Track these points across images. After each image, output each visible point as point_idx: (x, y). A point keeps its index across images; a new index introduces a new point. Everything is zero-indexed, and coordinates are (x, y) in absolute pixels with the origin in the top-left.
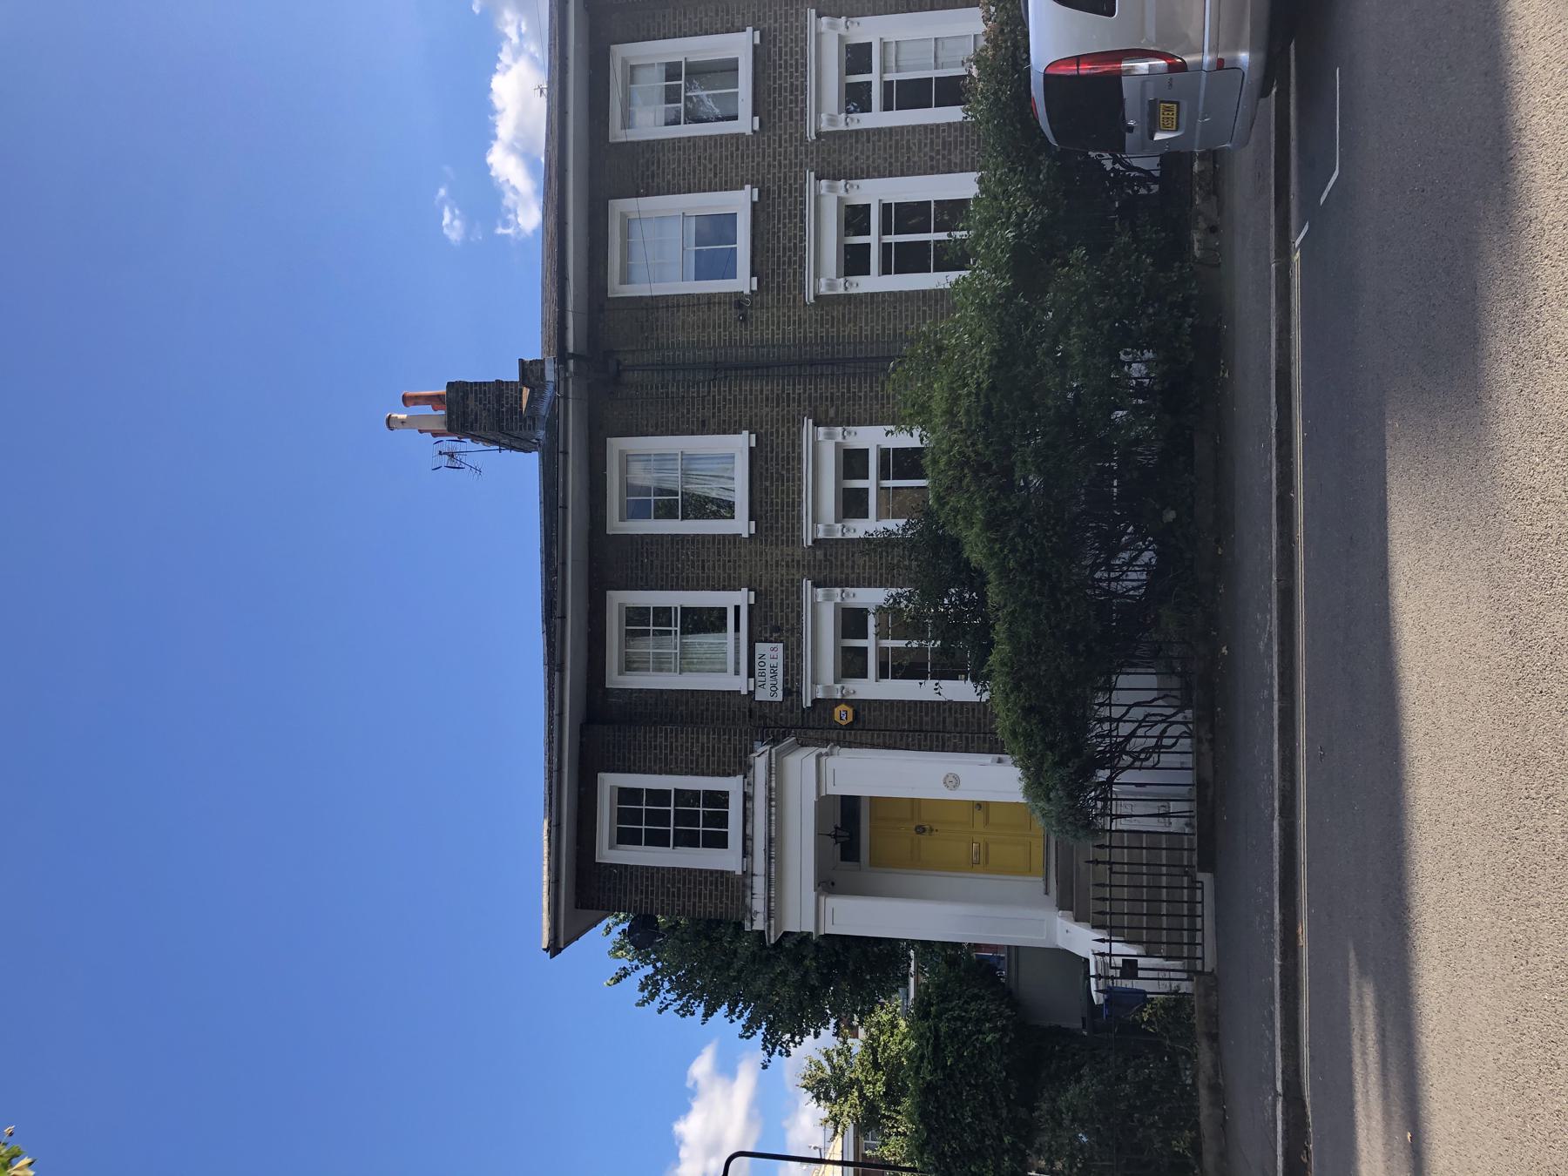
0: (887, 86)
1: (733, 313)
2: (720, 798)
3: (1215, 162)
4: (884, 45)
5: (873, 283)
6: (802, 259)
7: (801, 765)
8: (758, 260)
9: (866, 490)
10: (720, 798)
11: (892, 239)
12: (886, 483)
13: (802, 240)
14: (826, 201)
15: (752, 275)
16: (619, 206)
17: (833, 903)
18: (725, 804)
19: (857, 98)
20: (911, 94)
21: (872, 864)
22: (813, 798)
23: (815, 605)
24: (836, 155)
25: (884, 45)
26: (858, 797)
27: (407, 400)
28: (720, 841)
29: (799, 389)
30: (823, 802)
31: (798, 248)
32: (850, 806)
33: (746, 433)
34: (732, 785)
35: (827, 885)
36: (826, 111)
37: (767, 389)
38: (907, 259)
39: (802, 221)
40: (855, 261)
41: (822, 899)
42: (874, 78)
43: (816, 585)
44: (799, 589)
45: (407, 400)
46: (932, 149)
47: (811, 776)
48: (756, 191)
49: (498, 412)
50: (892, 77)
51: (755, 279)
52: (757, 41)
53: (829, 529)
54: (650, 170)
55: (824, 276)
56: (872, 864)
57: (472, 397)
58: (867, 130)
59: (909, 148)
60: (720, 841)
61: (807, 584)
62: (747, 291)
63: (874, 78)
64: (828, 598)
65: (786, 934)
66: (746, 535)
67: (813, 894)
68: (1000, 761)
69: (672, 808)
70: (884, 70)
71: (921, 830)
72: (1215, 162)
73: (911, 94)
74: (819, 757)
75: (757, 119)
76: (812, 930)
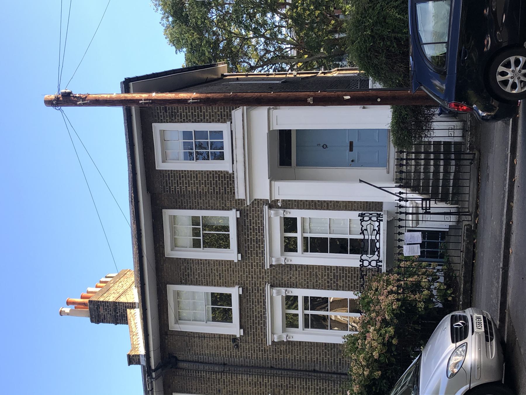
0: (305, 239)
1: (231, 344)
2: (220, 134)
3: (474, 248)
4: (303, 219)
5: (302, 335)
6: (265, 323)
7: (260, 113)
8: (243, 320)
9: (297, 315)
10: (220, 134)
11: (309, 312)
12: (307, 312)
13: (265, 314)
14: (276, 297)
15: (241, 328)
16: (171, 289)
17: (277, 184)
18: (222, 148)
19: (290, 246)
20: (317, 245)
21: (298, 165)
22: (267, 131)
23: (270, 218)
24: (280, 275)
25: (303, 219)
26: (291, 130)
27: (68, 303)
28: (221, 157)
29: (266, 380)
30: (271, 133)
31: (263, 316)
32: (284, 136)
33: (234, 210)
34: (223, 127)
35: (273, 176)
36: (274, 253)
37: (250, 379)
38: (319, 323)
39: (264, 304)
40: (291, 322)
41: (273, 182)
42: (298, 235)
43: (272, 286)
44: (262, 211)
45: (68, 303)
46: (328, 278)
47: (265, 121)
48: (241, 289)
49: (115, 316)
50: (309, 235)
51: (242, 330)
52: (238, 216)
53: (278, 260)
54: (189, 272)
55: (276, 331)
56: (298, 165)
57: (101, 307)
58: (296, 265)
59: (317, 276)
60: (221, 157)
61: (268, 287)
62: (236, 261)
63: (298, 235)
64: (278, 293)
65: (255, 200)
66: (236, 261)
67: (268, 181)
68: (364, 108)
69: (193, 141)
70: (304, 231)
71: (325, 146)
72: (474, 248)
73: (317, 245)
74: (269, 110)
75: (240, 255)
76: (268, 198)
